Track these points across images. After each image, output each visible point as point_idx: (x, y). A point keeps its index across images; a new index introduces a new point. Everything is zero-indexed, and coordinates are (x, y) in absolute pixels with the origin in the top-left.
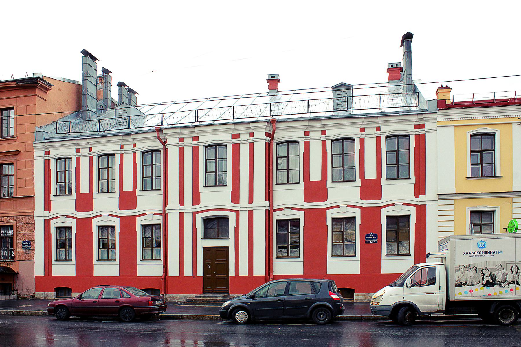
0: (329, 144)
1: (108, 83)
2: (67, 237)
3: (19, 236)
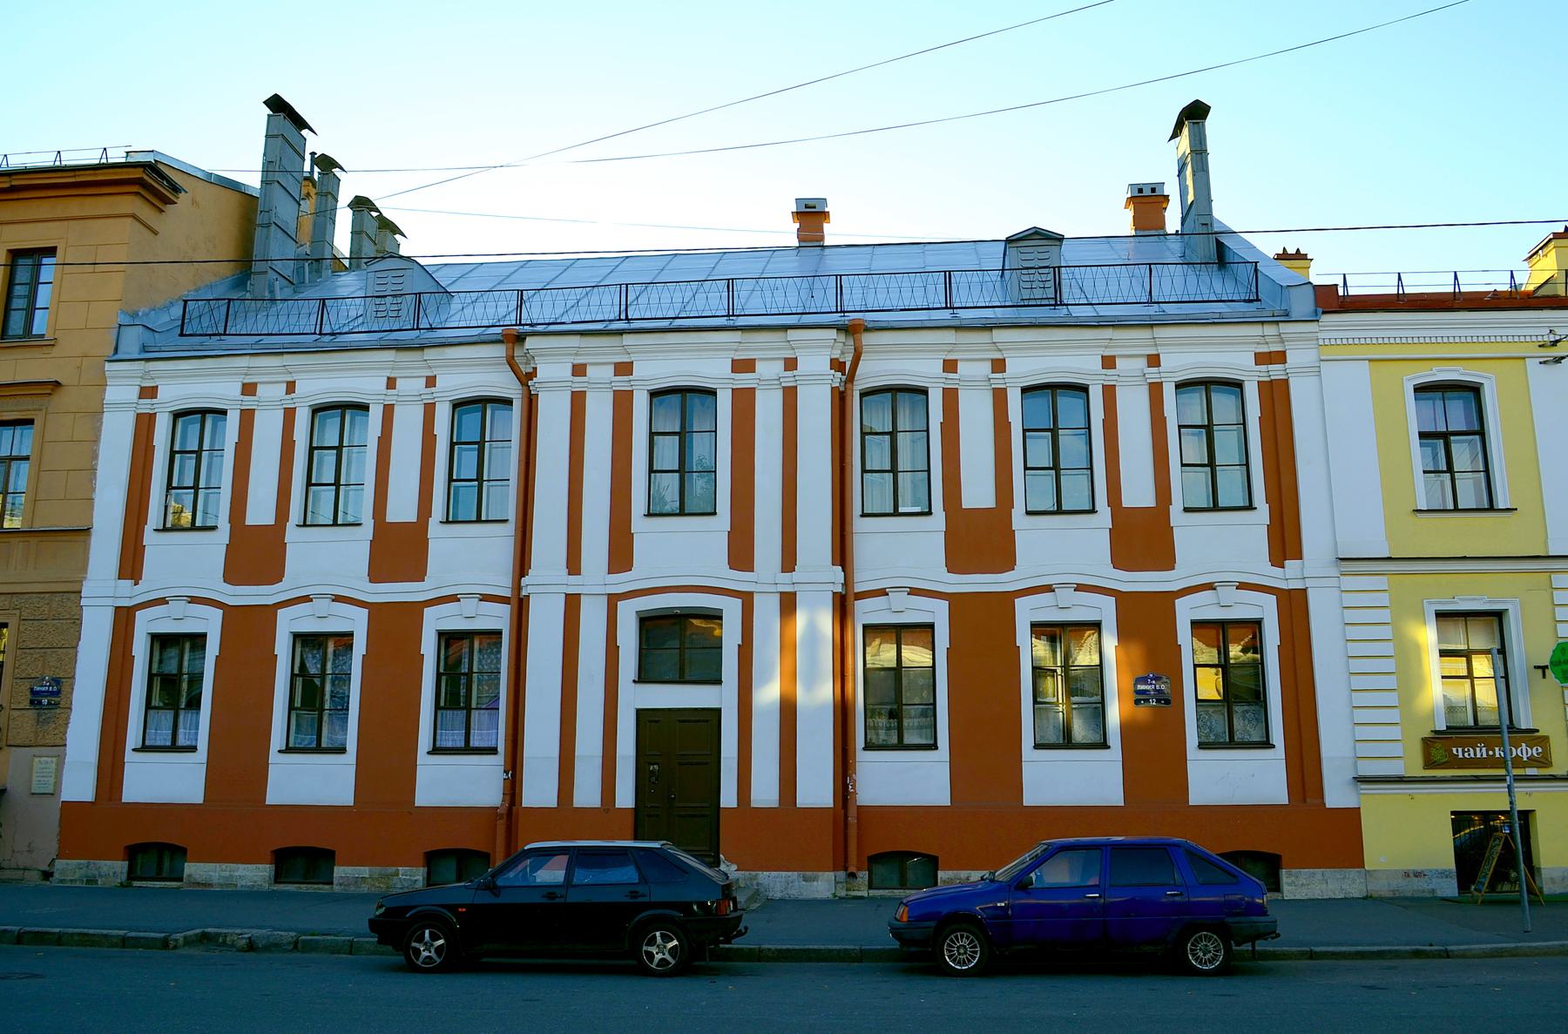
0: (1014, 400)
1: (329, 196)
2: (185, 670)
3: (24, 661)
